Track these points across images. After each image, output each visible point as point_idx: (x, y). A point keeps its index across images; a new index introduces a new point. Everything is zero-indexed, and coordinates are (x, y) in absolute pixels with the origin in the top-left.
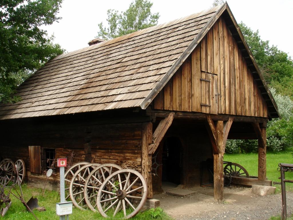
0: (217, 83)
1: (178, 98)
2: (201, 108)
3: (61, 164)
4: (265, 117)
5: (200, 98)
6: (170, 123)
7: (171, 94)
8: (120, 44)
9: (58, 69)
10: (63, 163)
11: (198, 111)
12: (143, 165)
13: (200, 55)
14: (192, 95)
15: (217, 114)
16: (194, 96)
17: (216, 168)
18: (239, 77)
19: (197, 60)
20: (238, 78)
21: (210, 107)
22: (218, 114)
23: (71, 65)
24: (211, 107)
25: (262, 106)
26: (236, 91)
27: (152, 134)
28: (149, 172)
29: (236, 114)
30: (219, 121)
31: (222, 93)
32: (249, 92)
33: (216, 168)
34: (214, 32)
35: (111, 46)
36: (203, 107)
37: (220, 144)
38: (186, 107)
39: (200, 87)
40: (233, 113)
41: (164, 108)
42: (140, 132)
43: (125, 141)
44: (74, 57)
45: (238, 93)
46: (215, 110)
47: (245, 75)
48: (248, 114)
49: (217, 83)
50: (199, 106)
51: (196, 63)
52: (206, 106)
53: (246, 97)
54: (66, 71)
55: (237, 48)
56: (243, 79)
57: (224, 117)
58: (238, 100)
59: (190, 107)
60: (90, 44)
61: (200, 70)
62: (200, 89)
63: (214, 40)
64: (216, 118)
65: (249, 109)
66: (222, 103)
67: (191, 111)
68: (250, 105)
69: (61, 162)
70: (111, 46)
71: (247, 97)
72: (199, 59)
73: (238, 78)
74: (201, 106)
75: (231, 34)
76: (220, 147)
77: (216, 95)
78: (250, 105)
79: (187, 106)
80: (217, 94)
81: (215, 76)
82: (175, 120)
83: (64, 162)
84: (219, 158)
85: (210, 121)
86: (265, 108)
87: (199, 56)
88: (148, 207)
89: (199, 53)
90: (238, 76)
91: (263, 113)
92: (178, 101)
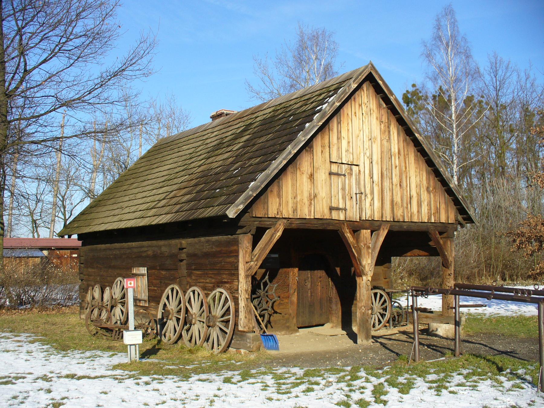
0: (359, 177)
1: (290, 201)
2: (331, 213)
3: (129, 285)
4: (450, 222)
5: (329, 200)
6: (279, 234)
7: (279, 196)
8: (240, 123)
9: (163, 159)
10: (131, 284)
11: (325, 218)
12: (240, 289)
13: (328, 139)
14: (315, 196)
15: (358, 220)
16: (318, 197)
17: (360, 296)
18: (400, 165)
19: (323, 146)
20: (396, 167)
21: (345, 210)
22: (360, 220)
23: (178, 152)
24: (348, 210)
25: (443, 206)
26: (394, 187)
27: (250, 248)
28: (247, 299)
29: (393, 219)
30: (362, 230)
31: (368, 191)
32: (419, 186)
33: (360, 296)
34: (353, 105)
35: (230, 124)
36: (333, 212)
37: (364, 263)
38: (305, 213)
39: (328, 183)
40: (388, 217)
41: (267, 214)
42: (235, 248)
43: (221, 259)
44: (184, 139)
45: (397, 190)
46: (353, 214)
47: (410, 162)
48: (415, 219)
49: (359, 177)
50: (327, 211)
51: (322, 152)
52: (338, 209)
53: (411, 194)
54: (171, 161)
55: (394, 124)
56: (406, 168)
57: (374, 226)
58: (397, 199)
59: (311, 212)
60: (214, 118)
61: (328, 161)
62: (328, 188)
63: (353, 116)
64: (356, 227)
65: (418, 212)
66: (368, 204)
67: (312, 217)
68: (419, 205)
69: (129, 282)
70: (230, 124)
71: (414, 193)
72: (327, 145)
73: (396, 167)
74: (331, 209)
75: (384, 105)
76: (365, 267)
77: (356, 194)
78: (419, 205)
79: (306, 211)
80: (357, 192)
81: (354, 167)
82: (285, 231)
83: (132, 282)
84: (364, 282)
85: (347, 231)
86: (449, 209)
87: (327, 141)
88: (458, 372)
89: (327, 137)
90: (397, 164)
91: (447, 215)
92: (290, 205)
